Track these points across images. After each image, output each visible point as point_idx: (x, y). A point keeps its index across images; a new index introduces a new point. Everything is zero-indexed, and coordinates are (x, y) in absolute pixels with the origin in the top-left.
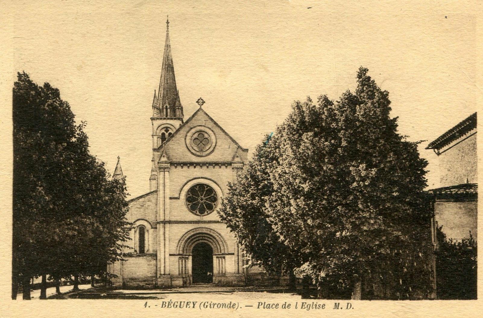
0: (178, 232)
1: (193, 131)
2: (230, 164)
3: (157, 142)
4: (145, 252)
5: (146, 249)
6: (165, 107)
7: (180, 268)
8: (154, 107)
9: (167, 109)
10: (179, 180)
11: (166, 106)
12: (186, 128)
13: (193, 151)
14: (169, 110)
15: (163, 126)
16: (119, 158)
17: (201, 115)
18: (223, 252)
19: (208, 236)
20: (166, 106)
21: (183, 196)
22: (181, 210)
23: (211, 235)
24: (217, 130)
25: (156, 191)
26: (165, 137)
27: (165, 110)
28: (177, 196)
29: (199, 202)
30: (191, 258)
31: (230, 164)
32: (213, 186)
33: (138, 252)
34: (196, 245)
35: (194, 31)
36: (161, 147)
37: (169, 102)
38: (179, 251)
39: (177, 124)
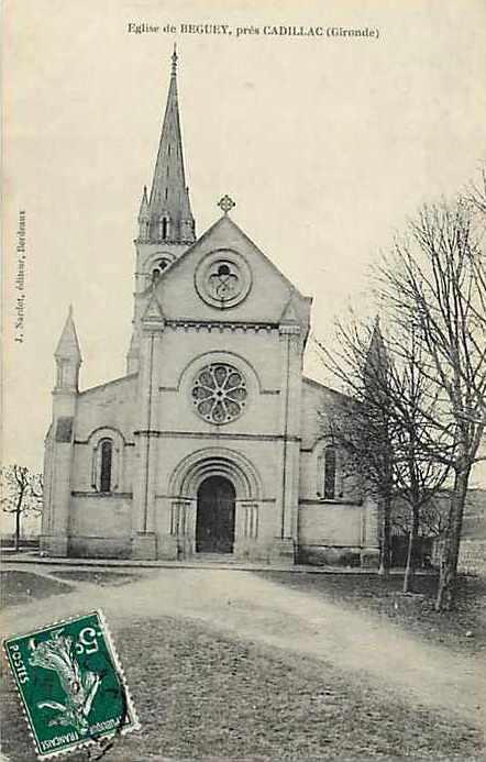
0: (175, 454)
1: (207, 261)
2: (275, 326)
3: (144, 283)
4: (111, 489)
5: (113, 484)
6: (161, 220)
7: (174, 525)
8: (141, 221)
9: (165, 222)
10: (186, 352)
11: (165, 219)
12: (196, 256)
13: (210, 301)
14: (168, 225)
15: (156, 257)
16: (71, 308)
17: (225, 225)
18: (253, 497)
19: (221, 462)
20: (165, 219)
21: (186, 387)
22: (179, 411)
23: (231, 462)
24: (251, 257)
25: (137, 375)
26: (159, 274)
27: (161, 225)
28: (175, 386)
29: (219, 403)
30: (194, 503)
31: (275, 326)
32: (245, 370)
33: (99, 489)
34: (207, 479)
35: (128, 468)
36: (149, 290)
37: (166, 222)
38: (173, 488)
39: (179, 251)
